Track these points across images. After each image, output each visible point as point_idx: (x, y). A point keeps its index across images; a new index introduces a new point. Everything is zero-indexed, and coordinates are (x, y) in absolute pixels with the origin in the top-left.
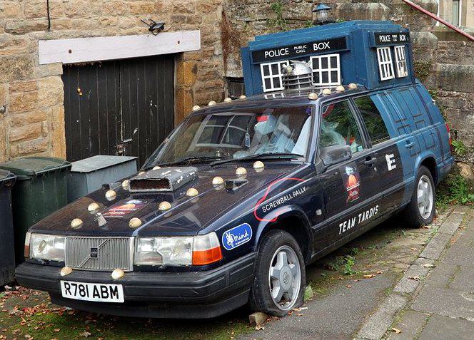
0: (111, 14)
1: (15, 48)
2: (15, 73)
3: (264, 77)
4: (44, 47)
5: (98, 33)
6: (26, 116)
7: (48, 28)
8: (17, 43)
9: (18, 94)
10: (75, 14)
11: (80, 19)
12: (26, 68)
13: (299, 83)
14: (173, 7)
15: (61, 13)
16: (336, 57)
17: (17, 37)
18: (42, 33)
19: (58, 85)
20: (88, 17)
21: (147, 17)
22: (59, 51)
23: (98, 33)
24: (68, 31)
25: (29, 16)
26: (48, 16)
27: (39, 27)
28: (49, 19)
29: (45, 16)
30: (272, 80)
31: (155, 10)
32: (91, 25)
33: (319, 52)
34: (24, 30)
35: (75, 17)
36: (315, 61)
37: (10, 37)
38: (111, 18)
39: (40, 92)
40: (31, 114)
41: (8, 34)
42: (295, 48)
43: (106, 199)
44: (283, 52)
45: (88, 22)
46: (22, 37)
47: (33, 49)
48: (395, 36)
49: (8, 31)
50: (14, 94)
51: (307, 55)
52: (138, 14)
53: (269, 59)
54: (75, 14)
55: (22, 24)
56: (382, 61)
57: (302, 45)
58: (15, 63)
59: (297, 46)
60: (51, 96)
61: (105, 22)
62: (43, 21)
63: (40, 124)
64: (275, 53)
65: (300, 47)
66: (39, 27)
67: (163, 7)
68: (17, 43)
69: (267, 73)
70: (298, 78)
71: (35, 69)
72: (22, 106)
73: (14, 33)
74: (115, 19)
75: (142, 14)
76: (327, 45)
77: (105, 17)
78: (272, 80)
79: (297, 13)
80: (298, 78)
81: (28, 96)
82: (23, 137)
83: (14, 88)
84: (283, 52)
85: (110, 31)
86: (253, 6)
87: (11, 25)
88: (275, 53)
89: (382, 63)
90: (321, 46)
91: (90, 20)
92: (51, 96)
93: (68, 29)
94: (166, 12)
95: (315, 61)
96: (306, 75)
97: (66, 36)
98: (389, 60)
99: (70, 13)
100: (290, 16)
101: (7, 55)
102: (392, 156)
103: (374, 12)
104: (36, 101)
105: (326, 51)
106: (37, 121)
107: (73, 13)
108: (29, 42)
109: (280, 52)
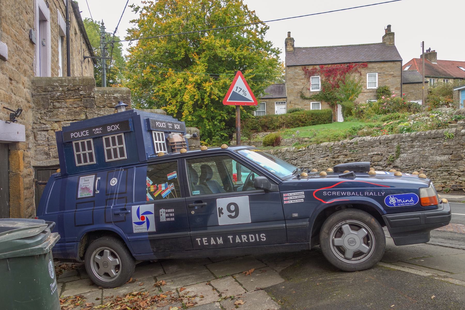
16: (121, 136)
30: (82, 155)
33: (111, 133)
42: (94, 130)
43: (229, 120)
44: (85, 133)
48: (230, 237)
56: (156, 140)
59: (95, 128)
64: (78, 134)
65: (97, 129)
70: (175, 144)
76: (117, 127)
78: (82, 155)
80: (175, 144)
84: (85, 133)
88: (78, 134)
89: (156, 142)
90: (113, 128)
96: (181, 142)
98: (163, 140)
102: (206, 239)
105: (116, 132)
109: (82, 133)
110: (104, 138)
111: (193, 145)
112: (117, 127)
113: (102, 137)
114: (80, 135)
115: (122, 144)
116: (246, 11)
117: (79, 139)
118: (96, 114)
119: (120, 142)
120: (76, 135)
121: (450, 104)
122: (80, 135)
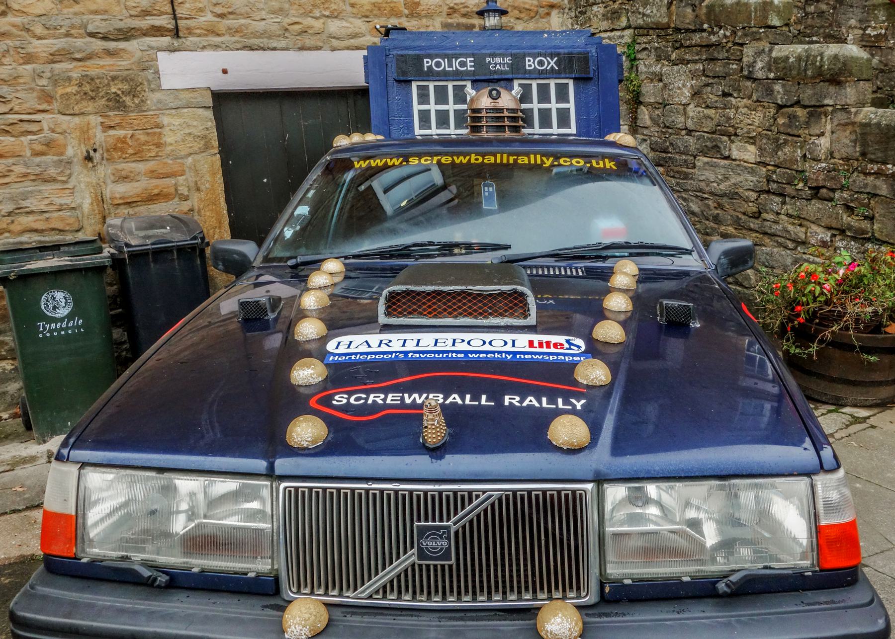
0: (307, 14)
1: (108, 61)
2: (109, 100)
3: (416, 107)
4: (164, 61)
5: (283, 43)
6: (141, 167)
7: (176, 33)
8: (109, 53)
9: (120, 133)
10: (230, 13)
11: (243, 21)
12: (132, 93)
13: (484, 123)
14: (445, 9)
15: (201, 10)
17: (112, 45)
18: (166, 40)
19: (204, 121)
20: (258, 18)
21: (379, 23)
22: (189, 71)
23: (283, 43)
24: (217, 40)
25: (133, 13)
26: (175, 15)
27: (157, 31)
28: (175, 18)
29: (167, 13)
31: (406, 12)
32: (265, 31)
34: (126, 35)
35: (231, 16)
36: (527, 89)
37: (98, 45)
38: (308, 21)
39: (165, 131)
40: (151, 165)
41: (93, 40)
42: (488, 60)
45: (260, 26)
46: (122, 45)
47: (148, 65)
49: (92, 35)
50: (112, 132)
51: (510, 76)
52: (367, 17)
53: (430, 75)
54: (230, 13)
55: (121, 25)
57: (503, 56)
58: (108, 85)
59: (494, 56)
60: (190, 139)
61: (297, 27)
62: (164, 21)
63: (172, 181)
64: (444, 64)
65: (498, 60)
66: (157, 31)
67: (421, 8)
68: (109, 53)
69: (424, 97)
70: (484, 114)
71: (152, 98)
72: (131, 151)
73: (105, 38)
74: (318, 24)
75: (376, 16)
76: (552, 63)
77: (296, 20)
79: (648, 16)
80: (506, 114)
81: (143, 138)
82: (139, 199)
83: (112, 124)
84: (463, 64)
85: (308, 41)
86: (595, 8)
87: (97, 24)
90: (541, 63)
91: (263, 23)
92: (190, 139)
93: (218, 35)
94: (429, 16)
95: (527, 89)
97: (216, 47)
99: (219, 10)
100: (640, 22)
101: (93, 72)
103: (755, 9)
104: (158, 145)
106: (167, 176)
107: (225, 11)
108: (138, 54)
110: (414, 85)
111: (826, 102)
112: (551, 63)
113: (410, 81)
114: (450, 65)
115: (448, 104)
116: (487, 271)
117: (445, 76)
118: (640, 13)
119: (562, 96)
120: (438, 65)
121: (362, 202)
122: (450, 65)
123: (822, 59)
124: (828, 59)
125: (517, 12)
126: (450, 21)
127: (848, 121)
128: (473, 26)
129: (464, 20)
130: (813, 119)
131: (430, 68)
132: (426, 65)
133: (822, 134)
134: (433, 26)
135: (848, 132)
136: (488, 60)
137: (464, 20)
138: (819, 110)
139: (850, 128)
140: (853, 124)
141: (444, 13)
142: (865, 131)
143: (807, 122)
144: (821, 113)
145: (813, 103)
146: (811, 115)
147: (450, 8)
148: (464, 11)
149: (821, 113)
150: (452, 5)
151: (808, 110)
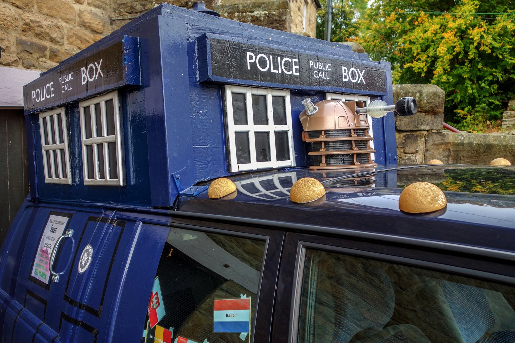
3: (233, 128)
14: (21, 23)
59: (318, 59)
111: (423, 127)
117: (272, 81)
122: (276, 67)
123: (421, 95)
124: (427, 95)
125: (79, 42)
126: (24, 38)
127: (442, 141)
128: (45, 48)
129: (36, 40)
130: (409, 141)
131: (253, 65)
132: (249, 61)
133: (417, 152)
134: (9, 41)
135: (441, 150)
136: (312, 63)
137: (36, 40)
138: (415, 134)
139: (443, 147)
140: (447, 144)
141: (20, 29)
142: (458, 149)
143: (403, 143)
144: (417, 136)
145: (410, 129)
146: (407, 138)
147: (26, 24)
148: (38, 30)
149: (417, 136)
150: (28, 21)
151: (404, 134)
